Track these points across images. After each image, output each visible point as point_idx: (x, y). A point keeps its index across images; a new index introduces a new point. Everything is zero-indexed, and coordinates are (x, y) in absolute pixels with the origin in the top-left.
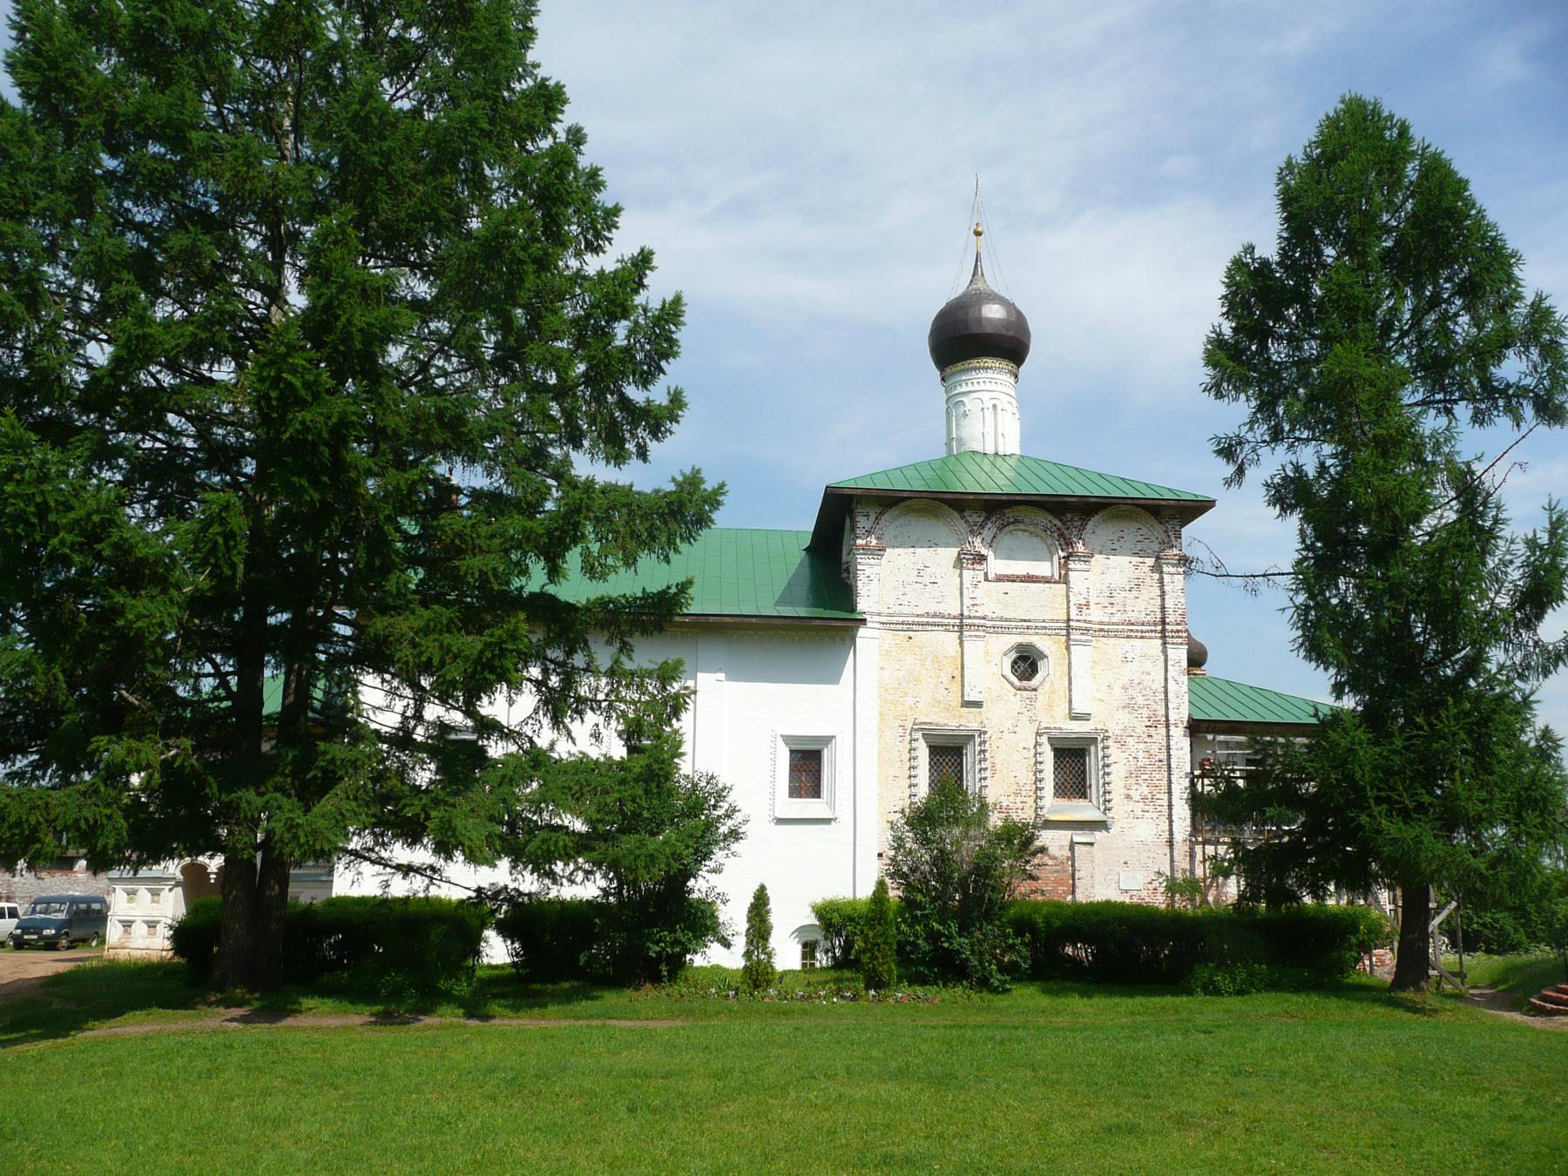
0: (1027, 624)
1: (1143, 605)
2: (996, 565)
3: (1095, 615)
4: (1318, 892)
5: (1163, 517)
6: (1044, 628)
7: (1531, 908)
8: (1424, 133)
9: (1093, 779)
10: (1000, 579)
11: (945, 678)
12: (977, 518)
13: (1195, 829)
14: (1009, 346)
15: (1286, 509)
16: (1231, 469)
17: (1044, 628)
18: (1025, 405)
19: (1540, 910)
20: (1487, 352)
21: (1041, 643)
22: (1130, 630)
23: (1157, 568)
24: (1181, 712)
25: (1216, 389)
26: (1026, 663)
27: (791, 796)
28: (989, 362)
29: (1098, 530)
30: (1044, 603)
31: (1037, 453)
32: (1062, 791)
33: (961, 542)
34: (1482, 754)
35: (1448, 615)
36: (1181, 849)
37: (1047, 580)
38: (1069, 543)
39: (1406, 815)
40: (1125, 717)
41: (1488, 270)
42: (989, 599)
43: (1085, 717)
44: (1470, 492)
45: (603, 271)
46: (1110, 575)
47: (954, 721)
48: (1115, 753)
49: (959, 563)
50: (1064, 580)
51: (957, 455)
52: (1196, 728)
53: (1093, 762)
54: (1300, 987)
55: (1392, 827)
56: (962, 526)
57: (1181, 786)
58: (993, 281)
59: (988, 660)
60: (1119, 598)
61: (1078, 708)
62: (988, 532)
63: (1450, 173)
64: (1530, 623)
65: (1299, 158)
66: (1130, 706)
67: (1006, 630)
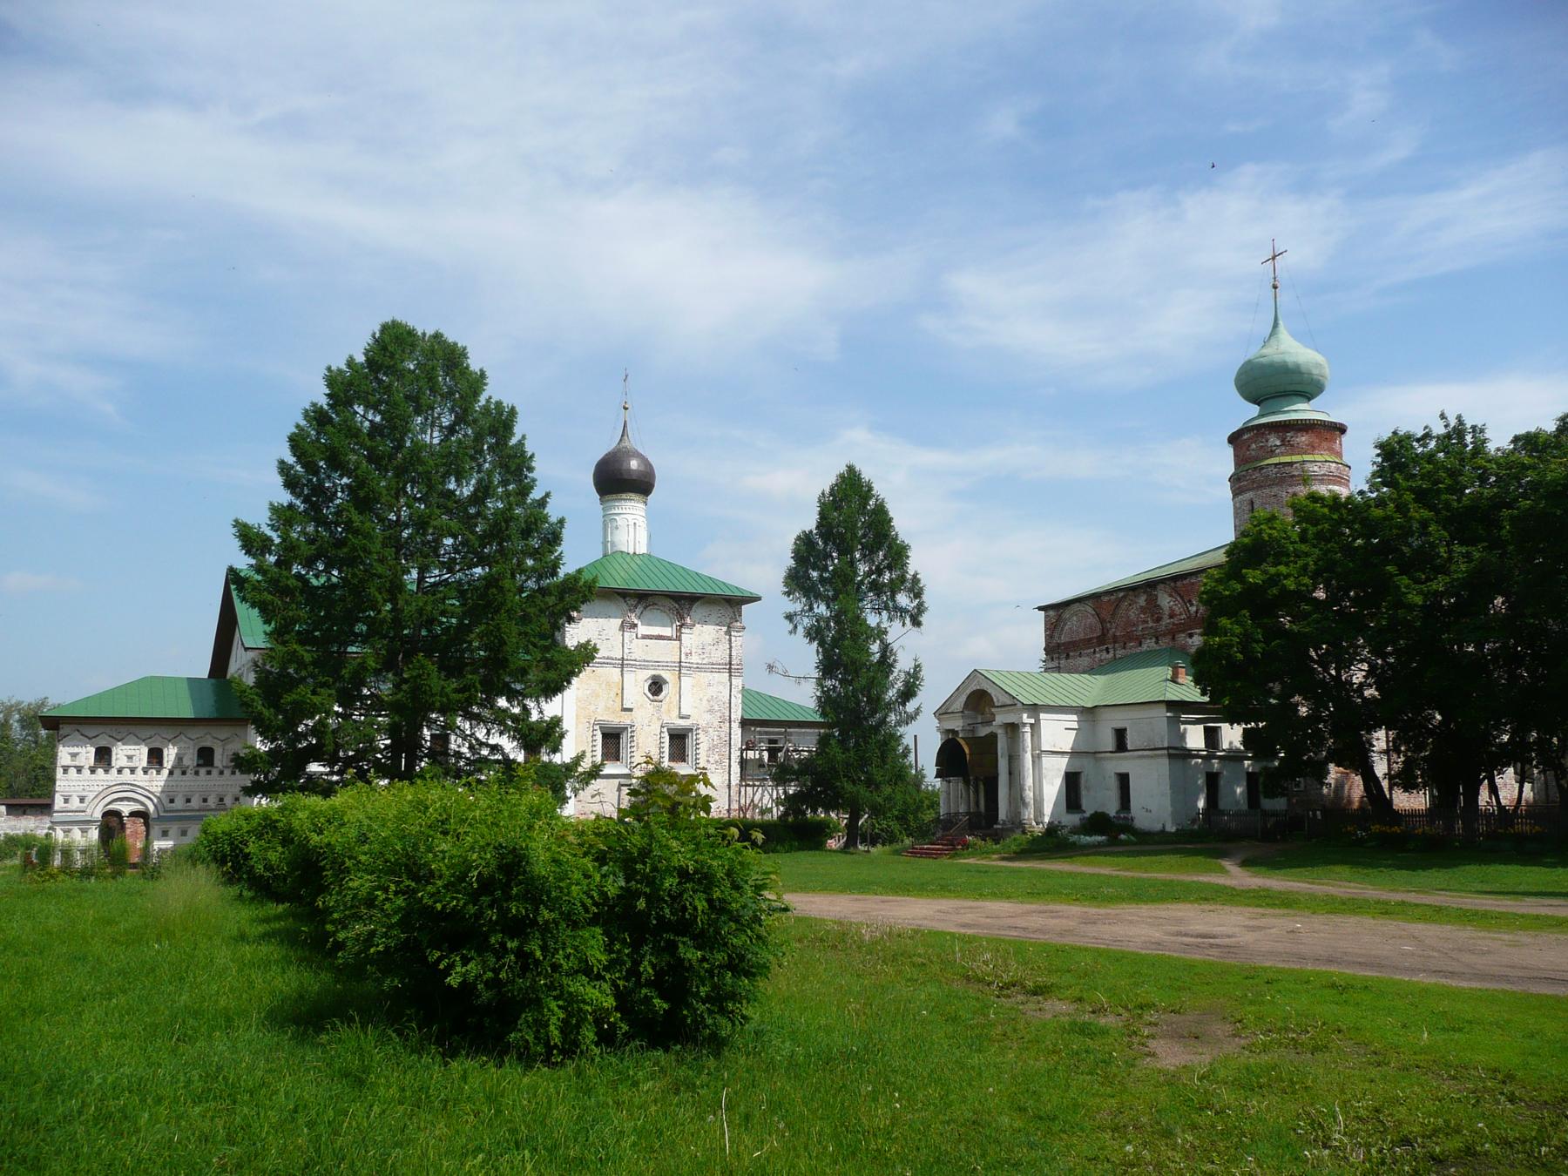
0: (658, 664)
1: (720, 654)
2: (643, 629)
3: (695, 659)
4: (814, 811)
5: (728, 605)
6: (666, 667)
7: (911, 817)
8: (879, 489)
9: (690, 751)
10: (644, 637)
11: (613, 694)
12: (633, 602)
13: (742, 778)
14: (641, 485)
15: (812, 640)
16: (791, 627)
17: (666, 667)
18: (650, 518)
19: (916, 819)
20: (894, 587)
21: (665, 675)
22: (713, 668)
23: (728, 633)
24: (737, 715)
25: (788, 594)
26: (656, 686)
27: (393, 342)
28: (633, 495)
29: (698, 611)
30: (665, 652)
31: (658, 554)
32: (672, 759)
33: (623, 615)
34: (883, 758)
35: (876, 703)
36: (734, 789)
37: (669, 639)
38: (682, 618)
39: (854, 782)
40: (707, 717)
41: (898, 555)
42: (638, 649)
43: (687, 717)
44: (886, 649)
45: (595, 580)
46: (702, 636)
47: (616, 719)
48: (702, 737)
49: (622, 628)
50: (679, 639)
51: (611, 556)
52: (745, 723)
53: (689, 742)
54: (810, 849)
55: (849, 787)
56: (625, 607)
57: (736, 755)
58: (635, 442)
59: (637, 683)
60: (708, 648)
61: (684, 712)
62: (638, 611)
63: (885, 513)
64: (904, 704)
65: (827, 491)
66: (711, 711)
67: (646, 668)
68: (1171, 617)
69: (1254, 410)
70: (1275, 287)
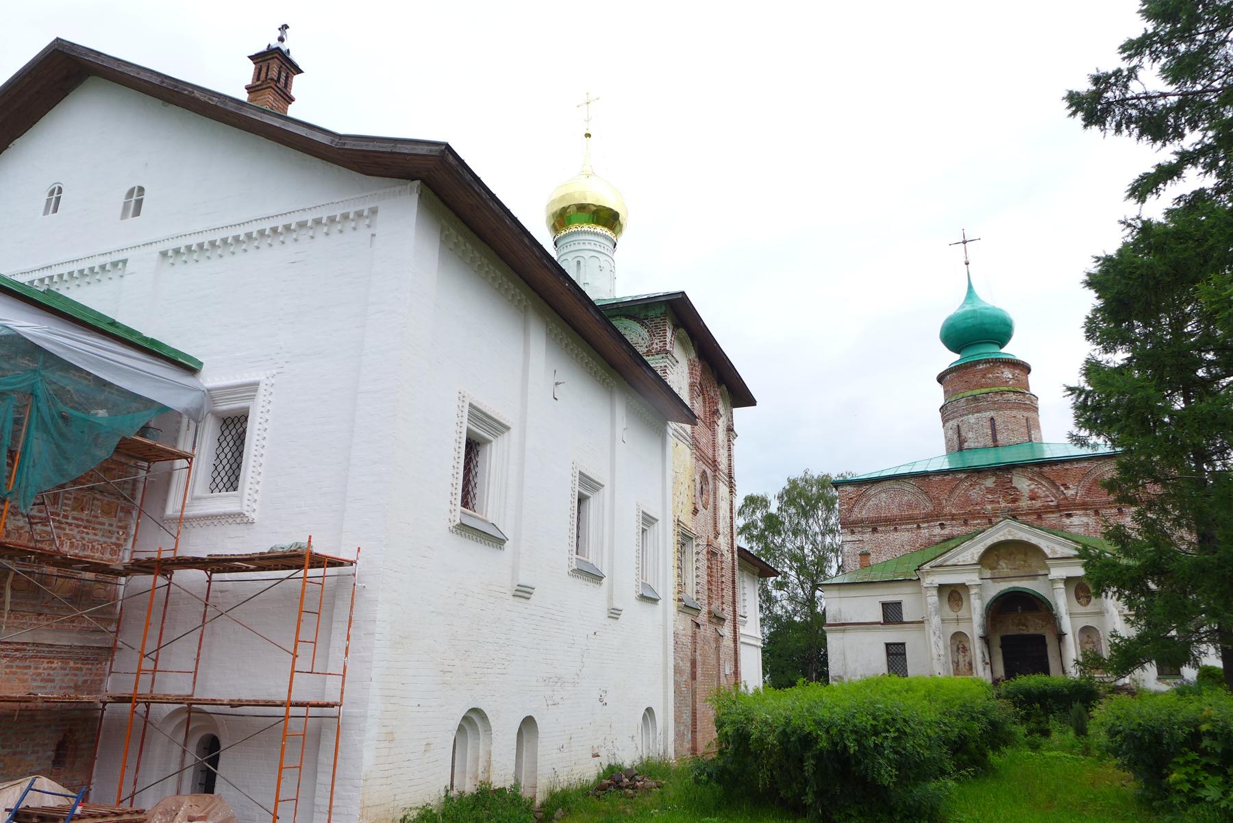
68: (1032, 498)
69: (957, 357)
70: (967, 264)
